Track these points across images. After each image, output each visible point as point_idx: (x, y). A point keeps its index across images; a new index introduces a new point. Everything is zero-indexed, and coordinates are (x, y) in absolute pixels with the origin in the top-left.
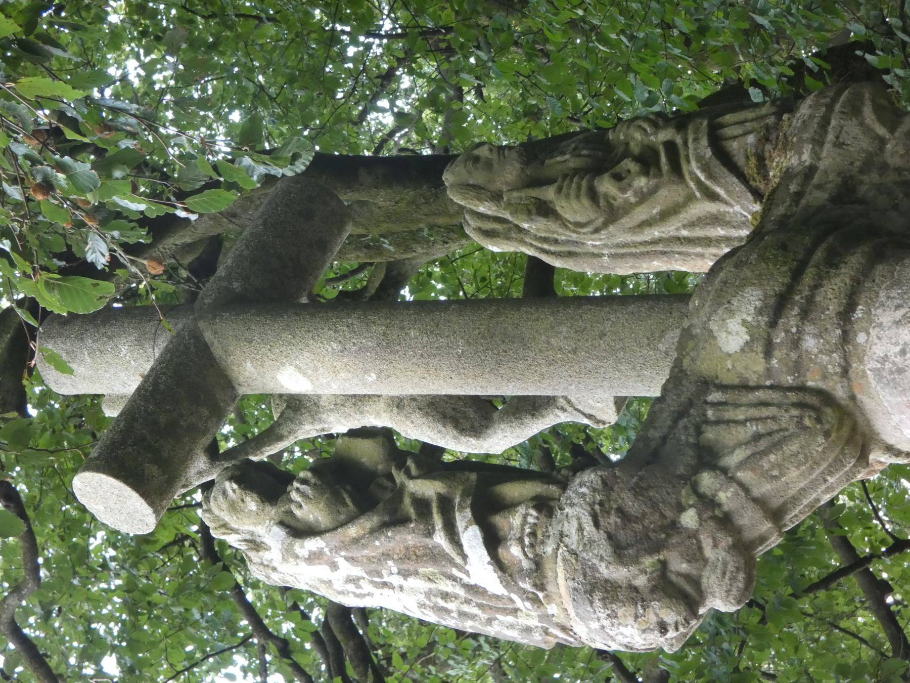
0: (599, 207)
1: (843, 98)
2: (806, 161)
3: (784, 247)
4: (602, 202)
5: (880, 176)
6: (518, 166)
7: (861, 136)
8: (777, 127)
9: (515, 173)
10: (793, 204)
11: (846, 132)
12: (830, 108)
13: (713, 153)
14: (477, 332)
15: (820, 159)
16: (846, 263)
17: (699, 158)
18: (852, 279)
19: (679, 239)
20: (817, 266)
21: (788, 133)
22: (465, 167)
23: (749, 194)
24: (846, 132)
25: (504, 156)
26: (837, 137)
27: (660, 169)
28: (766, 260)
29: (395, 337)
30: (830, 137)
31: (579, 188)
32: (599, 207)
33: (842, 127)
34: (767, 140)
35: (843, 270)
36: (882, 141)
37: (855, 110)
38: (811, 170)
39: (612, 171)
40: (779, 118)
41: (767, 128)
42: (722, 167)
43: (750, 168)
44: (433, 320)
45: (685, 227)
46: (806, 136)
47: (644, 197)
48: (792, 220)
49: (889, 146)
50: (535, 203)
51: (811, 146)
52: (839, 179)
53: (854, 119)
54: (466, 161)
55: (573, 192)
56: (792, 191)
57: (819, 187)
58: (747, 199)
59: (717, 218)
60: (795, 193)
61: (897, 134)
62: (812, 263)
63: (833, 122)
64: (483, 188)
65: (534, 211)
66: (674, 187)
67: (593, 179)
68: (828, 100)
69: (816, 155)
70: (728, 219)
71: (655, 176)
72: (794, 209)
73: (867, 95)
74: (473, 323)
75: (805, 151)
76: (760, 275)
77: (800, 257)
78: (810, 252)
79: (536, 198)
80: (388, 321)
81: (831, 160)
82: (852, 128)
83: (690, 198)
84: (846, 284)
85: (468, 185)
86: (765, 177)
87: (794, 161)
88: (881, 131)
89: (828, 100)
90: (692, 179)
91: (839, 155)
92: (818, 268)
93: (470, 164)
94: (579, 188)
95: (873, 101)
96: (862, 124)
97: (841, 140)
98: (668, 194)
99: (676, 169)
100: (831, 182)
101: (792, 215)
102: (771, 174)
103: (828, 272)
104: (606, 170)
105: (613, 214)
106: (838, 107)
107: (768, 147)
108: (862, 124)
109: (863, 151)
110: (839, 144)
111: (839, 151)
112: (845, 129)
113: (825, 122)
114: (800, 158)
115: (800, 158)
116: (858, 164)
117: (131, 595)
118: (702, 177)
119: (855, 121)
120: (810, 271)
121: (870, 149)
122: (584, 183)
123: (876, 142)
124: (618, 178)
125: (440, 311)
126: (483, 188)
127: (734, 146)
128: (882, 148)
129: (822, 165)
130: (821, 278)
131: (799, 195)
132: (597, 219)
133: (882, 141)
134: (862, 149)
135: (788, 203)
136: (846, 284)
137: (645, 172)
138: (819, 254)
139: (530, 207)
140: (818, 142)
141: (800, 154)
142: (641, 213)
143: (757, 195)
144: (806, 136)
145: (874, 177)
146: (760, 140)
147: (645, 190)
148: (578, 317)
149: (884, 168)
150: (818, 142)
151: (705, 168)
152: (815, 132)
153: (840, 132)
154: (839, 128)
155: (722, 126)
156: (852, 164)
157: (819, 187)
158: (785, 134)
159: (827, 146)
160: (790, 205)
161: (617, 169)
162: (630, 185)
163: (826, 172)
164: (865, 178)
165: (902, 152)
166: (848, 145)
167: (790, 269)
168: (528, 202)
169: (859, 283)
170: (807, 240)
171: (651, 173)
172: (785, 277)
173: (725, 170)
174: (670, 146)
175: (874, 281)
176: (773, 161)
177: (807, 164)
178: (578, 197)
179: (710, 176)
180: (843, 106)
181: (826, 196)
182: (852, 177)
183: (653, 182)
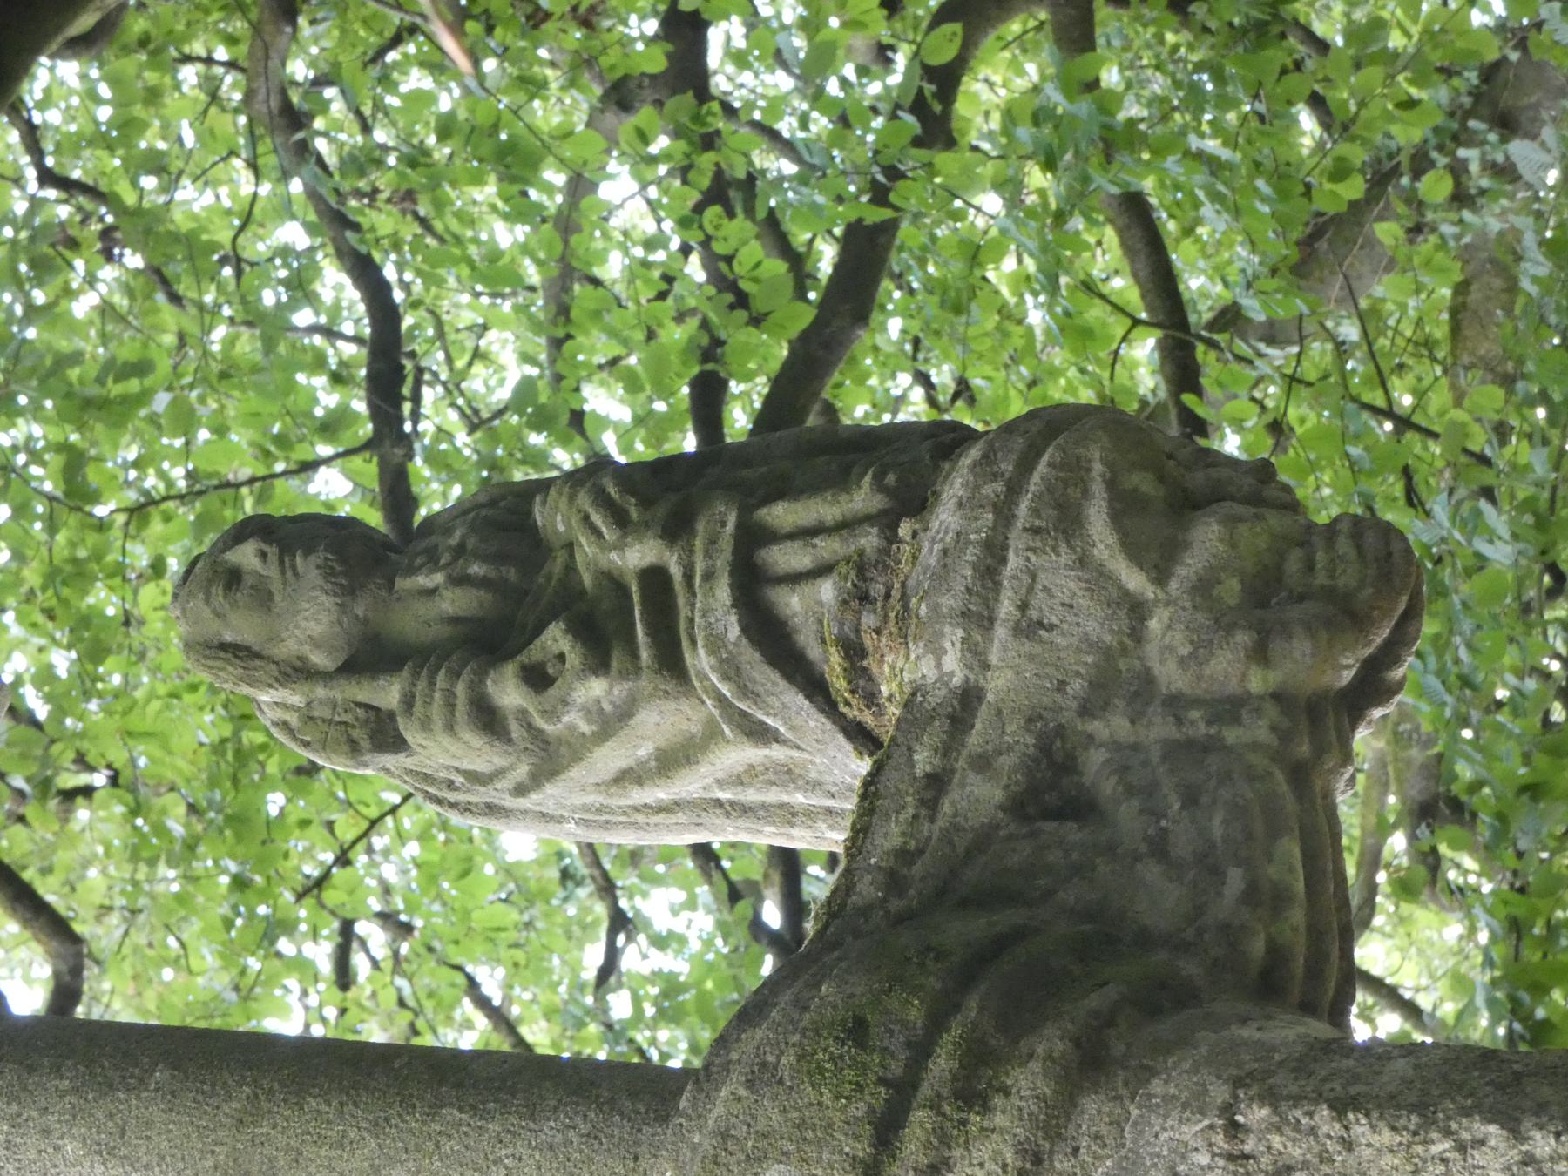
0: (509, 741)
1: (1036, 481)
2: (952, 674)
3: (857, 1031)
4: (516, 730)
5: (1133, 722)
6: (328, 601)
7: (1083, 602)
8: (885, 559)
9: (325, 618)
10: (924, 812)
11: (1045, 589)
12: (1004, 512)
13: (745, 630)
14: (210, 1163)
15: (986, 666)
16: (1006, 1092)
17: (716, 644)
18: (1021, 1151)
19: (719, 803)
20: (935, 1106)
21: (911, 583)
22: (207, 601)
23: (841, 738)
24: (1045, 589)
25: (296, 573)
26: (1023, 607)
27: (635, 655)
28: (817, 1074)
29: (33, 1155)
30: (1006, 607)
31: (450, 705)
32: (509, 741)
33: (1034, 577)
34: (864, 598)
35: (1000, 1120)
36: (1137, 610)
37: (1065, 521)
38: (969, 697)
39: (522, 658)
40: (891, 537)
41: (861, 566)
42: (768, 670)
43: (833, 666)
44: (111, 1116)
45: (720, 783)
46: (948, 602)
47: (610, 723)
48: (917, 869)
49: (1154, 624)
50: (367, 721)
51: (960, 633)
52: (1031, 741)
53: (1063, 547)
54: (210, 582)
55: (437, 711)
56: (919, 772)
57: (982, 763)
58: (840, 748)
59: (789, 772)
60: (928, 776)
61: (1174, 585)
62: (925, 1091)
63: (1014, 561)
64: (258, 656)
65: (365, 744)
66: (671, 705)
67: (481, 675)
68: (999, 487)
69: (976, 656)
70: (813, 775)
71: (624, 675)
72: (926, 827)
73: (1098, 467)
74: (200, 1137)
75: (948, 645)
76: (801, 1125)
77: (896, 1069)
78: (921, 1052)
79: (368, 707)
80: (15, 1108)
81: (1010, 674)
82: (1060, 579)
83: (711, 735)
84: (1004, 1166)
85: (224, 647)
86: (871, 699)
87: (927, 669)
88: (1135, 580)
89: (999, 487)
90: (706, 691)
91: (1031, 658)
92: (940, 1113)
93: (218, 592)
94: (450, 705)
95: (1111, 484)
96: (1083, 561)
97: (1034, 614)
98: (661, 721)
99: (672, 664)
100: (1010, 748)
101: (921, 852)
102: (884, 689)
103: (964, 1123)
104: (510, 656)
105: (550, 759)
106: (1023, 507)
107: (869, 620)
108: (1083, 561)
109: (1091, 645)
110: (1029, 628)
111: (1028, 647)
112: (1043, 579)
113: (995, 551)
114: (939, 665)
115: (939, 665)
116: (1076, 686)
117: (21, 811)
118: (725, 689)
119: (1066, 557)
120: (920, 1120)
121: (1107, 638)
122: (461, 689)
123: (1122, 613)
124: (537, 679)
125: (128, 1090)
126: (258, 656)
127: (793, 603)
128: (1137, 634)
129: (997, 684)
130: (946, 1141)
131: (937, 782)
132: (512, 768)
133: (1137, 610)
134: (1086, 638)
135: (911, 811)
136: (1004, 1166)
137: (599, 663)
138: (942, 1064)
139: (356, 734)
140: (979, 619)
141: (939, 653)
142: (610, 758)
143: (861, 736)
144: (948, 602)
145: (1115, 726)
146: (845, 602)
147: (607, 707)
148: (430, 1145)
149: (1143, 689)
150: (979, 619)
151: (731, 670)
152: (968, 590)
153: (1031, 589)
154: (1026, 579)
155: (772, 536)
156: (1061, 686)
157: (982, 763)
158: (903, 584)
159: (1001, 632)
160: (915, 817)
161: (534, 653)
162: (565, 703)
163: (999, 712)
164: (1095, 727)
165: (1185, 651)
166: (1051, 628)
167: (871, 1110)
168: (347, 718)
169: (1037, 1160)
170: (915, 1014)
171: (614, 664)
172: (856, 1137)
173: (775, 676)
174: (655, 577)
175: (1076, 1150)
176: (881, 661)
177: (957, 681)
178: (450, 727)
179: (744, 691)
180: (1035, 512)
181: (998, 795)
182: (1060, 730)
183: (621, 690)
